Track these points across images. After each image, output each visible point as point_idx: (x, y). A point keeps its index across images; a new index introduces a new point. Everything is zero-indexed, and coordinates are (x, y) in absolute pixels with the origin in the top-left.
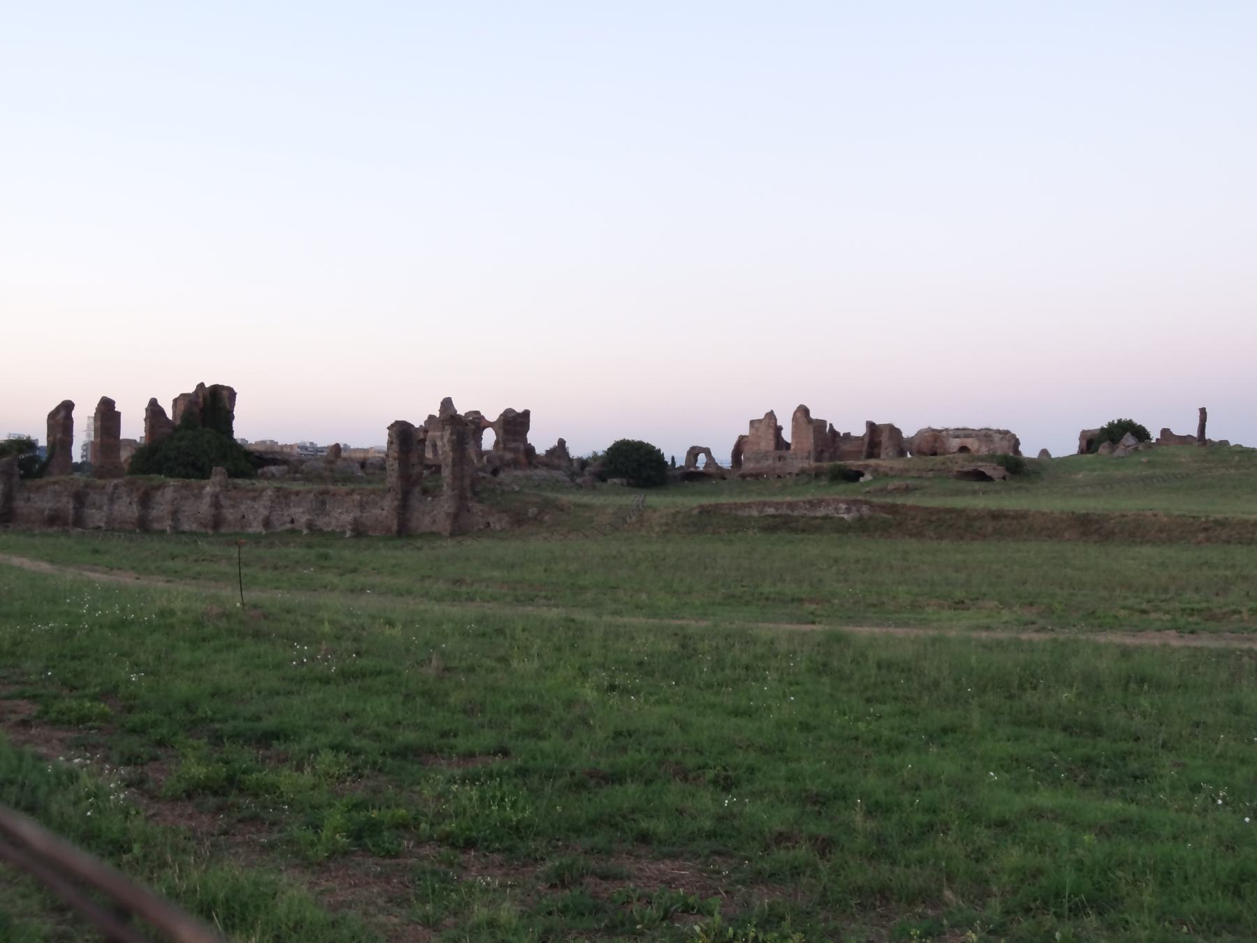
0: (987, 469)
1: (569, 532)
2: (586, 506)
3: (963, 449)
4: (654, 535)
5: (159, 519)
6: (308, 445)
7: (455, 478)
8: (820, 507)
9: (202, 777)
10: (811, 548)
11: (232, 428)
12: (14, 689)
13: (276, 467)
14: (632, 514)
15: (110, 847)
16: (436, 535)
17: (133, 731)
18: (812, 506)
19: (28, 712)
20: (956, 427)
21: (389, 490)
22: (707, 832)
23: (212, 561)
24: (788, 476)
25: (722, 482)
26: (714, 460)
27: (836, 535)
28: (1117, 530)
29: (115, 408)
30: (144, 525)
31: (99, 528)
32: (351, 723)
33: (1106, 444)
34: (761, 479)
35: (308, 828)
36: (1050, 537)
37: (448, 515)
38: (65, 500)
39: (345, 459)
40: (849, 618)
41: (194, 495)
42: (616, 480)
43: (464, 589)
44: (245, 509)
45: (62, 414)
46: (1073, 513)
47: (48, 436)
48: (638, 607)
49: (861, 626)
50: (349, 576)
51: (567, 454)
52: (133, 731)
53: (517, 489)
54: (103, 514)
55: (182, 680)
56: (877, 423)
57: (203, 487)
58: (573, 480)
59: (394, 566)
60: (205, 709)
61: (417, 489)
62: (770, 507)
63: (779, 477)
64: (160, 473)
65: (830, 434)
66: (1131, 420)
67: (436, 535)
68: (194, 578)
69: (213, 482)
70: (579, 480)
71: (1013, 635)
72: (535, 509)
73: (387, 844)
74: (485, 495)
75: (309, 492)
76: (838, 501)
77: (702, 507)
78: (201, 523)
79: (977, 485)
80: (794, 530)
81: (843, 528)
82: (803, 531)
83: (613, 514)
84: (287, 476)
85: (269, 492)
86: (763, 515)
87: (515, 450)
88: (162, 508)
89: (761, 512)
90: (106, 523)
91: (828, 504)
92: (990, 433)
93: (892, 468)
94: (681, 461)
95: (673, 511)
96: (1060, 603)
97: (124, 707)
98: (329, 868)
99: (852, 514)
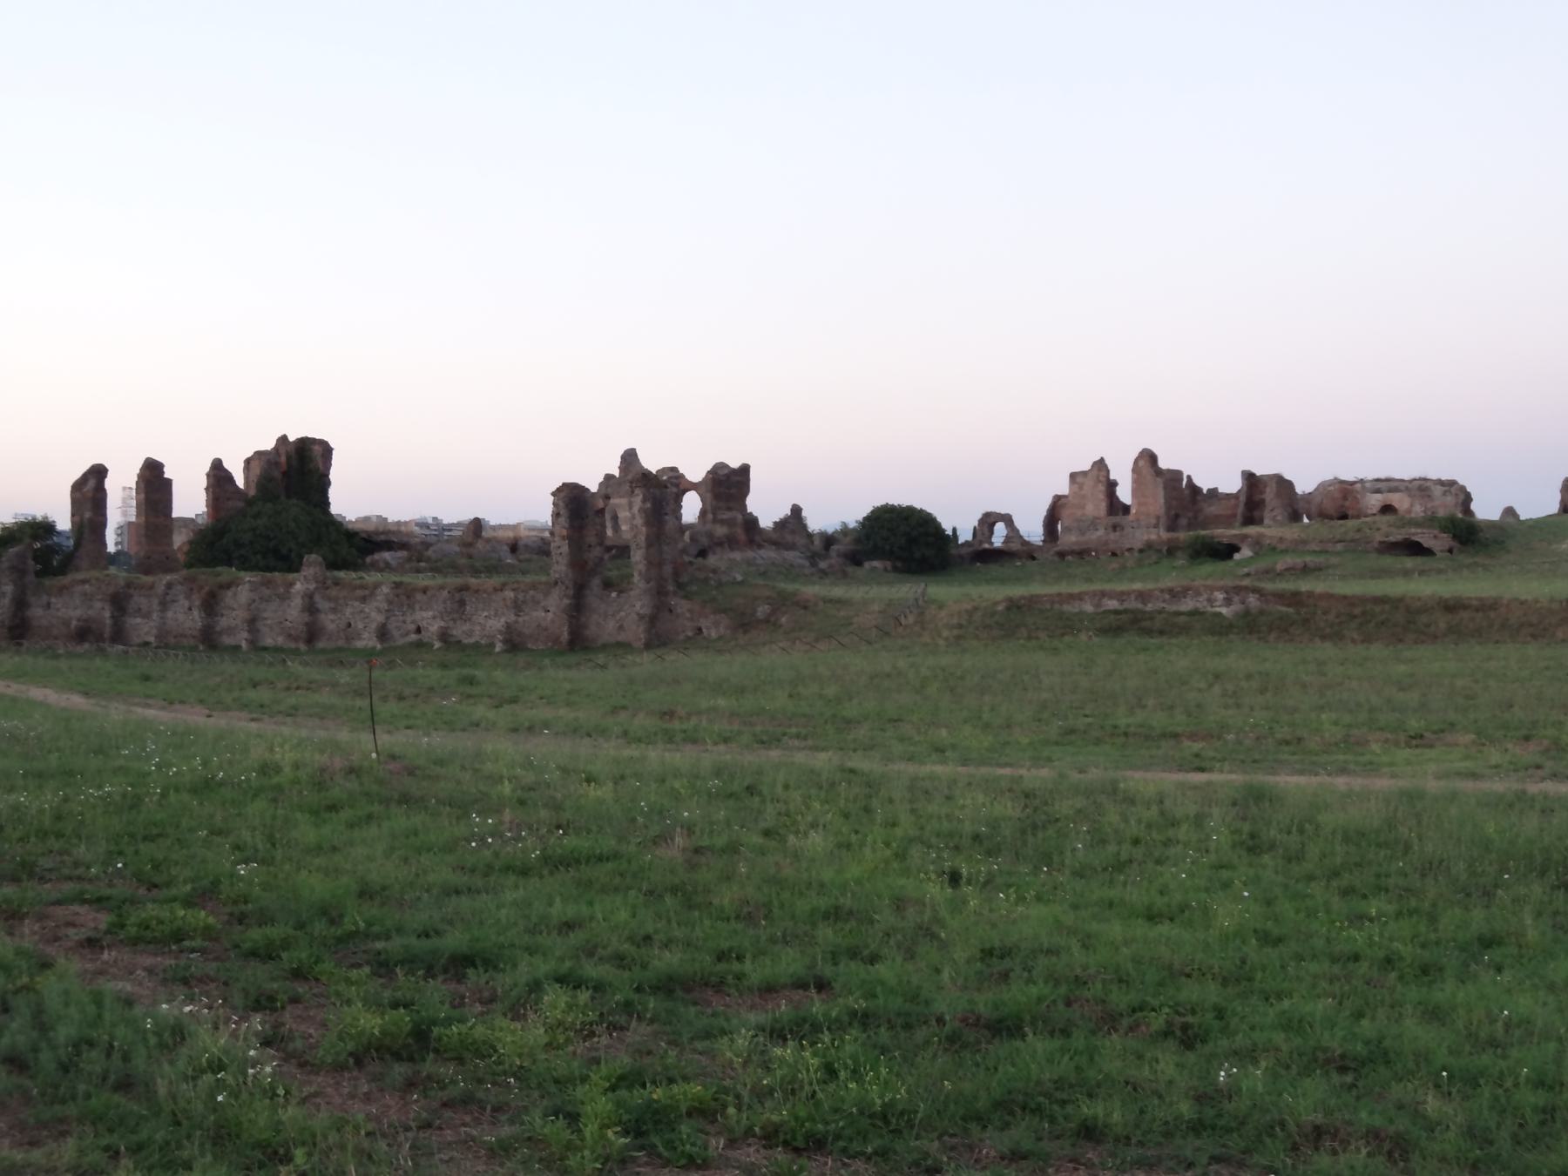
0: (1425, 538)
1: (817, 640)
3: (1387, 509)
4: (941, 642)
5: (230, 631)
6: (430, 521)
7: (650, 564)
8: (1185, 597)
9: (376, 1032)
11: (328, 498)
12: (69, 888)
13: (392, 553)
14: (908, 611)
15: (259, 1155)
16: (625, 646)
17: (253, 954)
18: (1174, 597)
19: (92, 925)
20: (1376, 477)
22: (1188, 1122)
23: (308, 689)
24: (1126, 553)
25: (1030, 563)
26: (1018, 531)
29: (163, 473)
30: (209, 639)
31: (146, 644)
32: (576, 938)
34: (1087, 558)
36: (1534, 636)
37: (641, 617)
38: (98, 605)
39: (488, 540)
40: (1255, 761)
41: (278, 596)
42: (876, 564)
43: (676, 725)
44: (352, 614)
45: (92, 483)
47: (73, 515)
48: (940, 750)
49: (1274, 774)
50: (506, 708)
51: (805, 527)
52: (253, 954)
54: (152, 624)
55: (310, 872)
56: (1258, 473)
57: (292, 584)
58: (814, 565)
59: (569, 693)
60: (356, 917)
61: (596, 582)
63: (1114, 554)
64: (230, 566)
65: (1187, 492)
67: (625, 646)
68: (290, 715)
69: (305, 576)
70: (823, 565)
71: (1516, 786)
72: (766, 607)
73: (688, 1147)
75: (442, 588)
76: (1212, 589)
77: (1010, 600)
78: (290, 636)
79: (1410, 562)
80: (1148, 632)
81: (1220, 628)
82: (1161, 633)
83: (880, 612)
84: (407, 566)
85: (385, 589)
87: (730, 523)
89: (1098, 605)
90: (156, 637)
91: (1198, 594)
92: (1428, 484)
93: (1281, 539)
94: (965, 536)
95: (969, 607)
97: (231, 914)
99: (1232, 607)
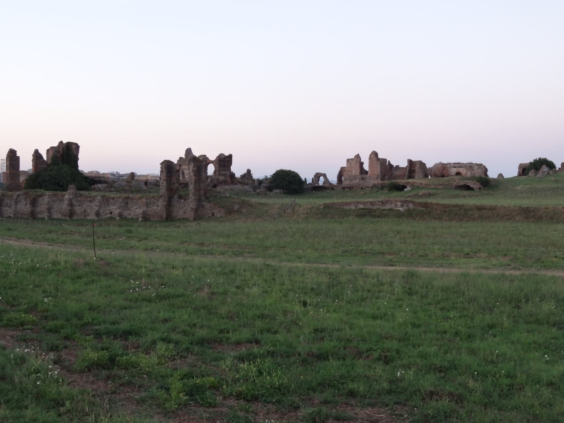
0: (471, 184)
1: (256, 218)
2: (264, 204)
3: (458, 174)
4: (300, 219)
5: (41, 212)
6: (115, 173)
7: (196, 190)
8: (387, 204)
9: (96, 359)
10: (385, 226)
13: (101, 185)
14: (289, 208)
15: (52, 403)
16: (187, 220)
17: (50, 330)
18: (383, 204)
20: (454, 162)
21: (161, 197)
23: (70, 234)
24: (367, 188)
25: (332, 191)
26: (328, 179)
27: (395, 219)
28: (543, 216)
30: (33, 215)
31: (10, 217)
32: (168, 325)
33: (533, 171)
34: (353, 190)
35: (162, 390)
36: (508, 219)
37: (192, 209)
39: (137, 181)
40: (411, 263)
42: (277, 191)
43: (205, 248)
44: (87, 207)
46: (520, 207)
48: (299, 258)
49: (418, 267)
50: (143, 242)
51: (252, 177)
52: (50, 330)
53: (228, 195)
54: (12, 210)
56: (413, 160)
57: (64, 196)
58: (255, 191)
60: (88, 317)
61: (176, 197)
62: (361, 204)
63: (362, 188)
65: (388, 167)
66: (546, 158)
67: (187, 220)
70: (258, 191)
71: (501, 272)
72: (238, 206)
73: (209, 400)
74: (212, 199)
75: (119, 198)
76: (397, 201)
77: (325, 204)
79: (466, 193)
80: (374, 216)
81: (399, 215)
82: (379, 217)
83: (279, 208)
84: (107, 190)
85: (99, 198)
86: (358, 208)
87: (224, 175)
88: (43, 206)
89: (356, 207)
90: (13, 214)
91: (392, 203)
92: (473, 165)
94: (309, 181)
96: (520, 254)
97: (42, 316)
98: (179, 414)
